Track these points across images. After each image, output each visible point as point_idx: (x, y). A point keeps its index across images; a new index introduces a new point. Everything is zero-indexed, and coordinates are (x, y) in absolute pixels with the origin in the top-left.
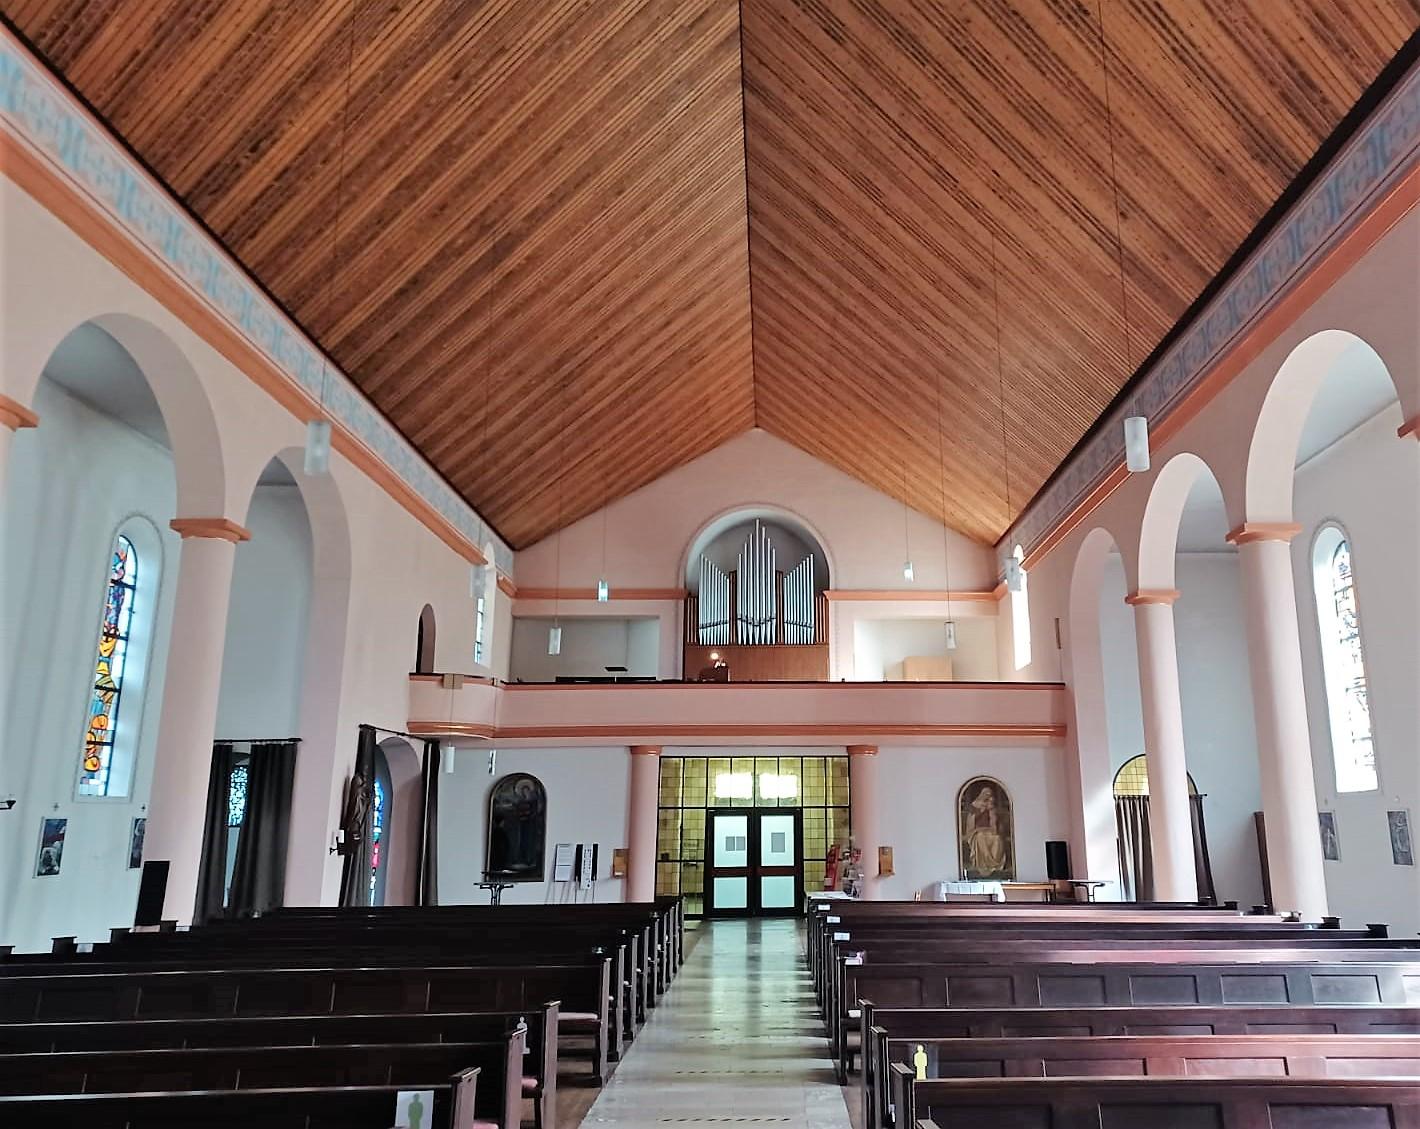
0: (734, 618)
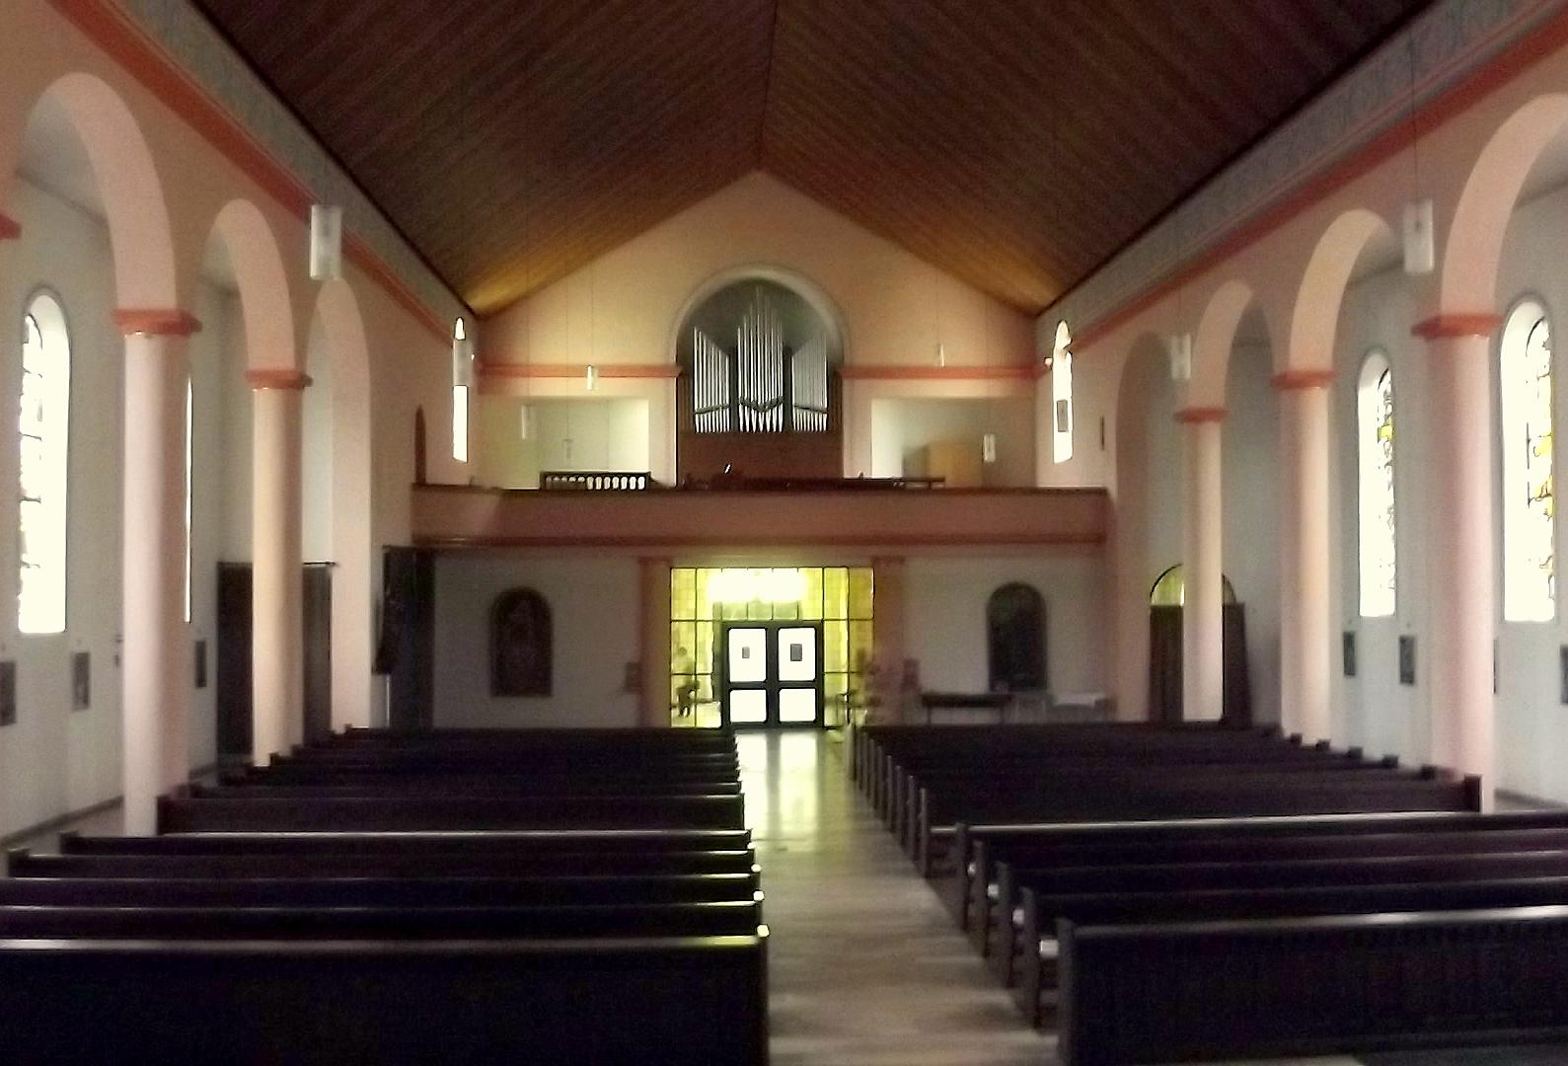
0: (733, 407)
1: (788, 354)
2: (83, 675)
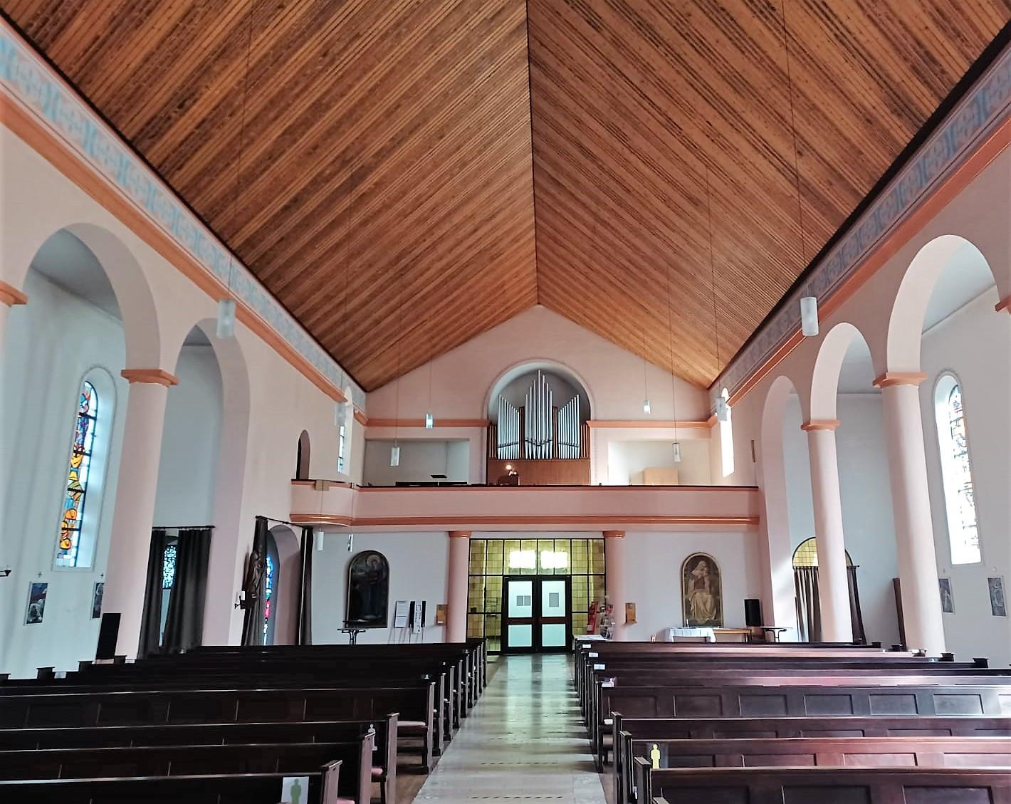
0: (523, 440)
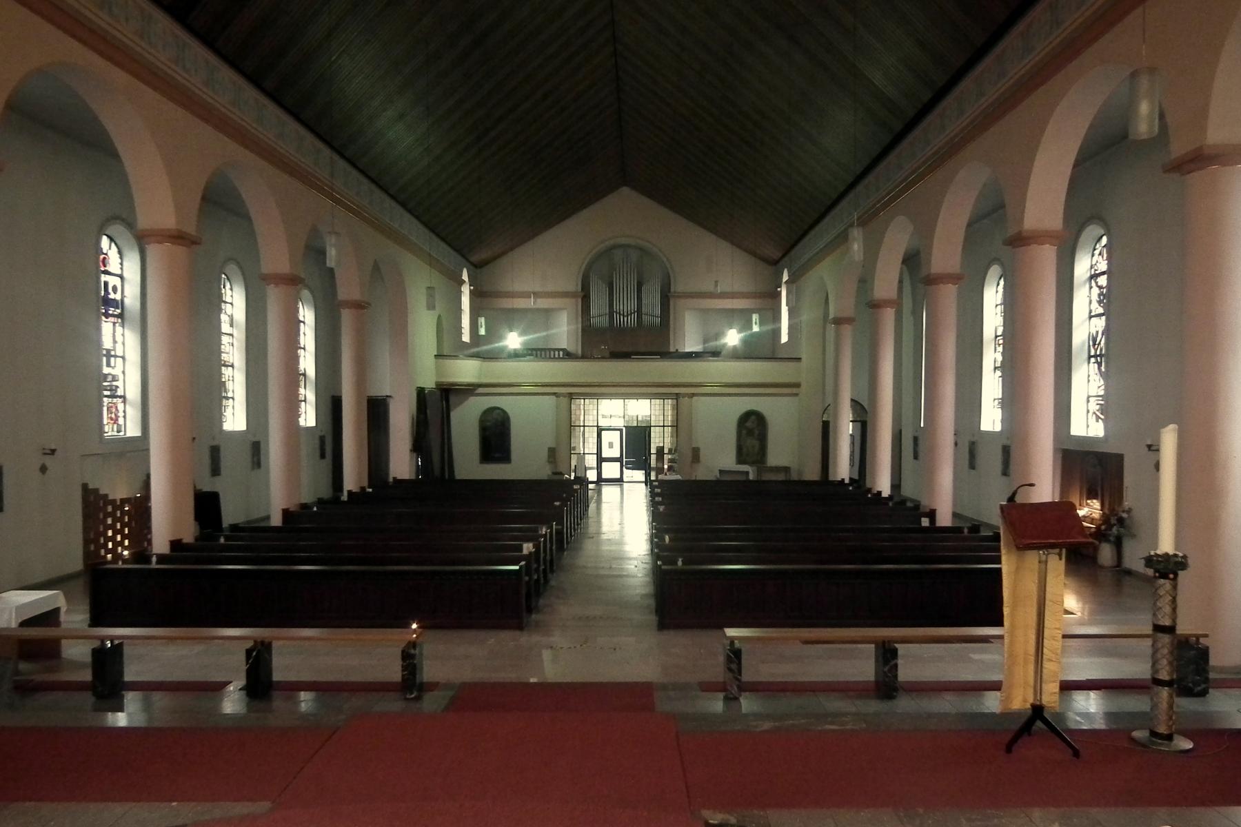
1: (640, 285)
2: (255, 449)
